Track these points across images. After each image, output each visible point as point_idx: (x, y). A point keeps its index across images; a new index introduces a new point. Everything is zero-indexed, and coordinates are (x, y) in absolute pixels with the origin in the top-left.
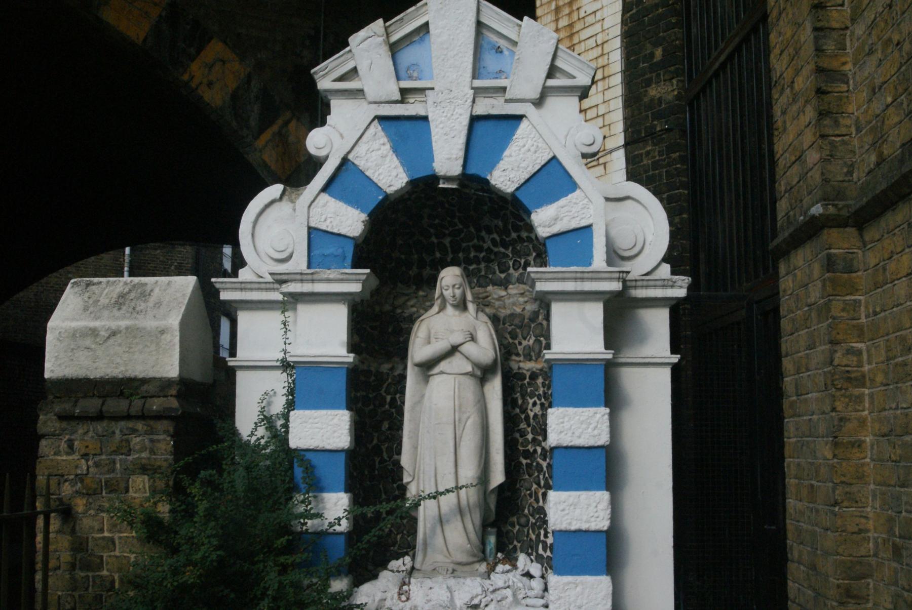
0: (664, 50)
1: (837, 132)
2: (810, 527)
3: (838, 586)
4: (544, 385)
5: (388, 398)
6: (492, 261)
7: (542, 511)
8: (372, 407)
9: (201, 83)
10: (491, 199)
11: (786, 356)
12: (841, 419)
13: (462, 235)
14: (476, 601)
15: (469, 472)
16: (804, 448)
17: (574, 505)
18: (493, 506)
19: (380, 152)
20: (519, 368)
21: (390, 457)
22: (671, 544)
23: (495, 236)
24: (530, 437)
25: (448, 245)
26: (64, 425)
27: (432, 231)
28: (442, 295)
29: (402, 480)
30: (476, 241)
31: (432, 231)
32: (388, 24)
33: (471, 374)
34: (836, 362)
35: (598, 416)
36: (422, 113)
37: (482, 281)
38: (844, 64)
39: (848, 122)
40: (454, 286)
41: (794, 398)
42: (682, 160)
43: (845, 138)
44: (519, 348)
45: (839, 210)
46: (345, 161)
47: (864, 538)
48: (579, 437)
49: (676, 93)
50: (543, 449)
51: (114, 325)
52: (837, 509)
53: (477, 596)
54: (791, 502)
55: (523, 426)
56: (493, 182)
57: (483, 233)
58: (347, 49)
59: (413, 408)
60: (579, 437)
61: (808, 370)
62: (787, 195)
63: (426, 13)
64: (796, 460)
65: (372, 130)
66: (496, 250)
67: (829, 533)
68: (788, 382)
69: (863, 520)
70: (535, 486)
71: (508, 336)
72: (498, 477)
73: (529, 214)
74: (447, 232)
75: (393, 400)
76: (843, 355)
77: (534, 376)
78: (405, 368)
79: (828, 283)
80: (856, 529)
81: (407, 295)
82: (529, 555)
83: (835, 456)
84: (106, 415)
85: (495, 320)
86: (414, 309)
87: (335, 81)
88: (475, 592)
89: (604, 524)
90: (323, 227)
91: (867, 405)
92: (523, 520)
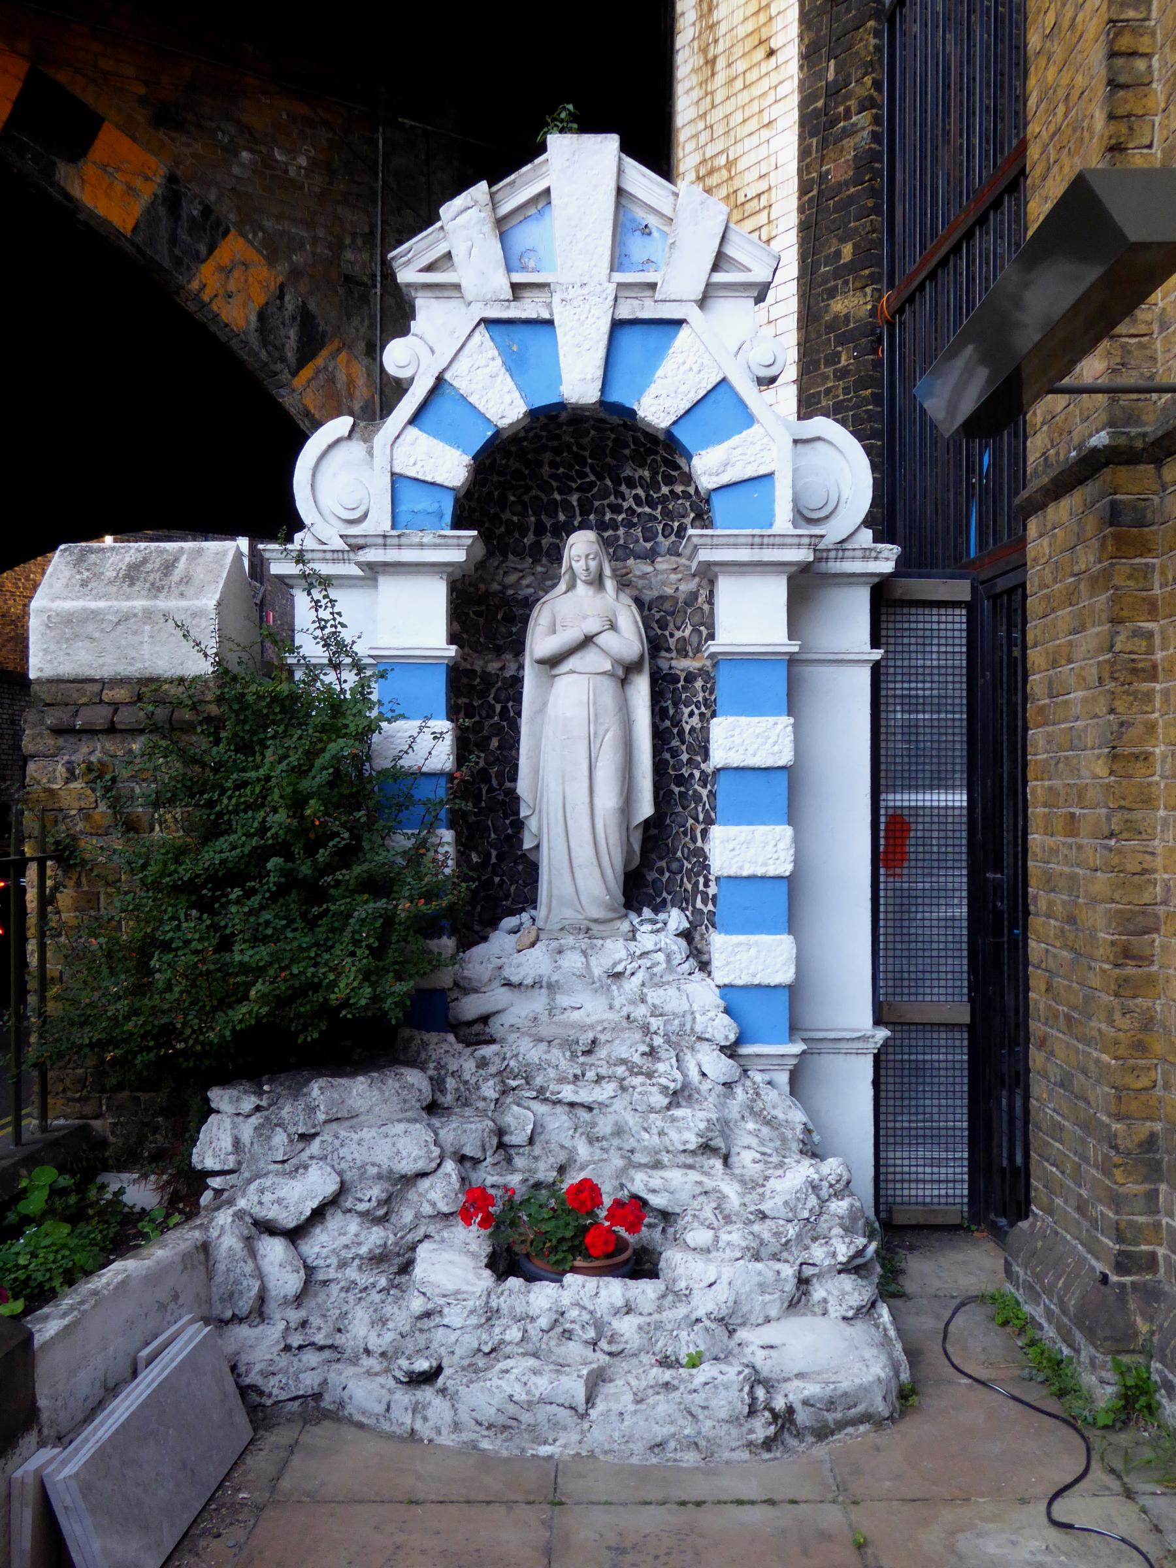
0: (855, 246)
1: (1132, 331)
2: (1067, 870)
3: (1113, 943)
4: (704, 689)
5: (498, 707)
6: (635, 525)
7: (701, 854)
8: (477, 718)
10: (636, 441)
11: (1035, 646)
12: (1122, 724)
14: (619, 969)
15: (608, 799)
16: (1061, 765)
17: (748, 843)
18: (637, 847)
19: (487, 370)
20: (671, 668)
21: (501, 784)
23: (640, 491)
24: (685, 757)
26: (60, 742)
27: (554, 484)
28: (571, 568)
29: (518, 813)
31: (554, 484)
32: (495, 188)
33: (610, 674)
34: (1117, 648)
35: (779, 727)
36: (546, 315)
37: (620, 553)
39: (1149, 316)
41: (1047, 701)
42: (877, 399)
43: (1143, 339)
45: (1132, 439)
46: (440, 381)
47: (1149, 881)
48: (754, 755)
49: (869, 307)
50: (703, 772)
51: (125, 605)
52: (1112, 842)
53: (621, 961)
54: (1036, 839)
55: (675, 743)
56: (641, 413)
57: (623, 488)
58: (438, 225)
59: (532, 719)
60: (754, 755)
61: (1070, 661)
62: (1045, 428)
63: (545, 175)
64: (1047, 783)
65: (477, 337)
66: (639, 510)
67: (1099, 874)
68: (1036, 681)
69: (1148, 857)
70: (691, 821)
71: (655, 626)
72: (645, 808)
73: (689, 457)
74: (574, 485)
75: (505, 709)
76: (1128, 638)
77: (690, 678)
78: (521, 667)
79: (1110, 542)
80: (1138, 869)
82: (683, 910)
83: (1112, 773)
84: (119, 727)
85: (639, 602)
86: (531, 590)
88: (617, 957)
89: (786, 869)
90: (412, 474)
91: (1158, 705)
92: (675, 866)
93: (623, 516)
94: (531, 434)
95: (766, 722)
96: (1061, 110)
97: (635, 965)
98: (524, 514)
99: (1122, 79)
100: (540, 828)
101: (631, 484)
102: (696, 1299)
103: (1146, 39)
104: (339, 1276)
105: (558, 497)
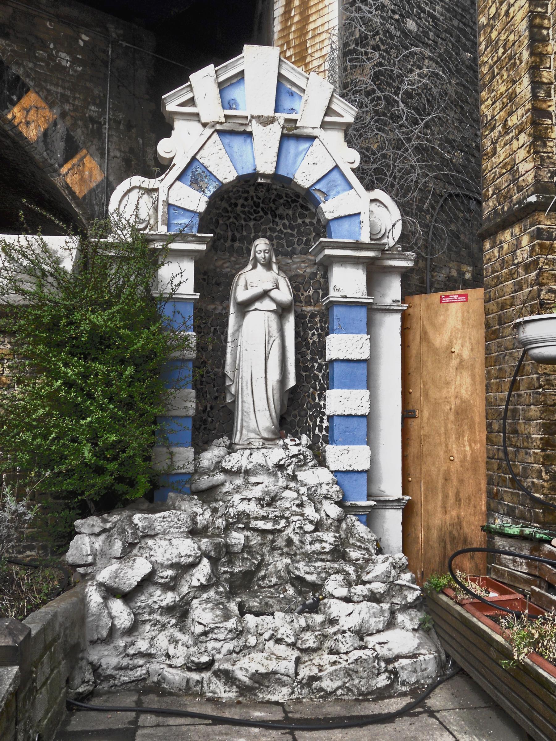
5: (212, 329)
6: (283, 238)
9: (21, 122)
13: (263, 220)
14: (282, 462)
15: (274, 375)
16: (507, 358)
18: (286, 402)
20: (302, 311)
22: (401, 428)
24: (309, 357)
25: (252, 227)
28: (255, 258)
30: (271, 224)
34: (542, 297)
38: (550, 106)
40: (264, 251)
41: (498, 327)
44: (302, 297)
52: (541, 390)
57: (277, 220)
58: (188, 84)
59: (233, 334)
62: (495, 196)
66: (285, 231)
67: (532, 407)
70: (312, 390)
72: (292, 382)
77: (313, 316)
81: (224, 259)
86: (229, 270)
87: (178, 105)
92: (303, 413)
93: (276, 234)
94: (234, 190)
95: (357, 337)
96: (501, 50)
97: (289, 461)
98: (226, 231)
99: (537, 37)
100: (237, 391)
101: (281, 218)
102: (341, 622)
103: (546, 21)
104: (151, 618)
105: (243, 222)
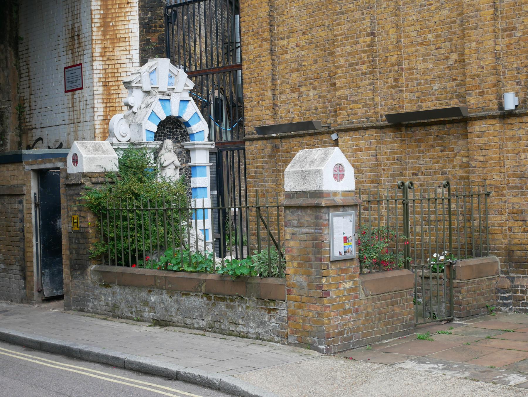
23: (169, 130)
26: (94, 185)
101: (167, 128)
